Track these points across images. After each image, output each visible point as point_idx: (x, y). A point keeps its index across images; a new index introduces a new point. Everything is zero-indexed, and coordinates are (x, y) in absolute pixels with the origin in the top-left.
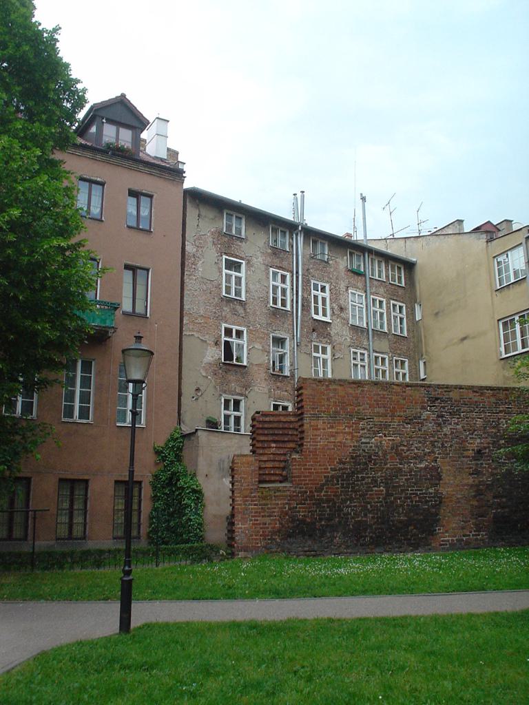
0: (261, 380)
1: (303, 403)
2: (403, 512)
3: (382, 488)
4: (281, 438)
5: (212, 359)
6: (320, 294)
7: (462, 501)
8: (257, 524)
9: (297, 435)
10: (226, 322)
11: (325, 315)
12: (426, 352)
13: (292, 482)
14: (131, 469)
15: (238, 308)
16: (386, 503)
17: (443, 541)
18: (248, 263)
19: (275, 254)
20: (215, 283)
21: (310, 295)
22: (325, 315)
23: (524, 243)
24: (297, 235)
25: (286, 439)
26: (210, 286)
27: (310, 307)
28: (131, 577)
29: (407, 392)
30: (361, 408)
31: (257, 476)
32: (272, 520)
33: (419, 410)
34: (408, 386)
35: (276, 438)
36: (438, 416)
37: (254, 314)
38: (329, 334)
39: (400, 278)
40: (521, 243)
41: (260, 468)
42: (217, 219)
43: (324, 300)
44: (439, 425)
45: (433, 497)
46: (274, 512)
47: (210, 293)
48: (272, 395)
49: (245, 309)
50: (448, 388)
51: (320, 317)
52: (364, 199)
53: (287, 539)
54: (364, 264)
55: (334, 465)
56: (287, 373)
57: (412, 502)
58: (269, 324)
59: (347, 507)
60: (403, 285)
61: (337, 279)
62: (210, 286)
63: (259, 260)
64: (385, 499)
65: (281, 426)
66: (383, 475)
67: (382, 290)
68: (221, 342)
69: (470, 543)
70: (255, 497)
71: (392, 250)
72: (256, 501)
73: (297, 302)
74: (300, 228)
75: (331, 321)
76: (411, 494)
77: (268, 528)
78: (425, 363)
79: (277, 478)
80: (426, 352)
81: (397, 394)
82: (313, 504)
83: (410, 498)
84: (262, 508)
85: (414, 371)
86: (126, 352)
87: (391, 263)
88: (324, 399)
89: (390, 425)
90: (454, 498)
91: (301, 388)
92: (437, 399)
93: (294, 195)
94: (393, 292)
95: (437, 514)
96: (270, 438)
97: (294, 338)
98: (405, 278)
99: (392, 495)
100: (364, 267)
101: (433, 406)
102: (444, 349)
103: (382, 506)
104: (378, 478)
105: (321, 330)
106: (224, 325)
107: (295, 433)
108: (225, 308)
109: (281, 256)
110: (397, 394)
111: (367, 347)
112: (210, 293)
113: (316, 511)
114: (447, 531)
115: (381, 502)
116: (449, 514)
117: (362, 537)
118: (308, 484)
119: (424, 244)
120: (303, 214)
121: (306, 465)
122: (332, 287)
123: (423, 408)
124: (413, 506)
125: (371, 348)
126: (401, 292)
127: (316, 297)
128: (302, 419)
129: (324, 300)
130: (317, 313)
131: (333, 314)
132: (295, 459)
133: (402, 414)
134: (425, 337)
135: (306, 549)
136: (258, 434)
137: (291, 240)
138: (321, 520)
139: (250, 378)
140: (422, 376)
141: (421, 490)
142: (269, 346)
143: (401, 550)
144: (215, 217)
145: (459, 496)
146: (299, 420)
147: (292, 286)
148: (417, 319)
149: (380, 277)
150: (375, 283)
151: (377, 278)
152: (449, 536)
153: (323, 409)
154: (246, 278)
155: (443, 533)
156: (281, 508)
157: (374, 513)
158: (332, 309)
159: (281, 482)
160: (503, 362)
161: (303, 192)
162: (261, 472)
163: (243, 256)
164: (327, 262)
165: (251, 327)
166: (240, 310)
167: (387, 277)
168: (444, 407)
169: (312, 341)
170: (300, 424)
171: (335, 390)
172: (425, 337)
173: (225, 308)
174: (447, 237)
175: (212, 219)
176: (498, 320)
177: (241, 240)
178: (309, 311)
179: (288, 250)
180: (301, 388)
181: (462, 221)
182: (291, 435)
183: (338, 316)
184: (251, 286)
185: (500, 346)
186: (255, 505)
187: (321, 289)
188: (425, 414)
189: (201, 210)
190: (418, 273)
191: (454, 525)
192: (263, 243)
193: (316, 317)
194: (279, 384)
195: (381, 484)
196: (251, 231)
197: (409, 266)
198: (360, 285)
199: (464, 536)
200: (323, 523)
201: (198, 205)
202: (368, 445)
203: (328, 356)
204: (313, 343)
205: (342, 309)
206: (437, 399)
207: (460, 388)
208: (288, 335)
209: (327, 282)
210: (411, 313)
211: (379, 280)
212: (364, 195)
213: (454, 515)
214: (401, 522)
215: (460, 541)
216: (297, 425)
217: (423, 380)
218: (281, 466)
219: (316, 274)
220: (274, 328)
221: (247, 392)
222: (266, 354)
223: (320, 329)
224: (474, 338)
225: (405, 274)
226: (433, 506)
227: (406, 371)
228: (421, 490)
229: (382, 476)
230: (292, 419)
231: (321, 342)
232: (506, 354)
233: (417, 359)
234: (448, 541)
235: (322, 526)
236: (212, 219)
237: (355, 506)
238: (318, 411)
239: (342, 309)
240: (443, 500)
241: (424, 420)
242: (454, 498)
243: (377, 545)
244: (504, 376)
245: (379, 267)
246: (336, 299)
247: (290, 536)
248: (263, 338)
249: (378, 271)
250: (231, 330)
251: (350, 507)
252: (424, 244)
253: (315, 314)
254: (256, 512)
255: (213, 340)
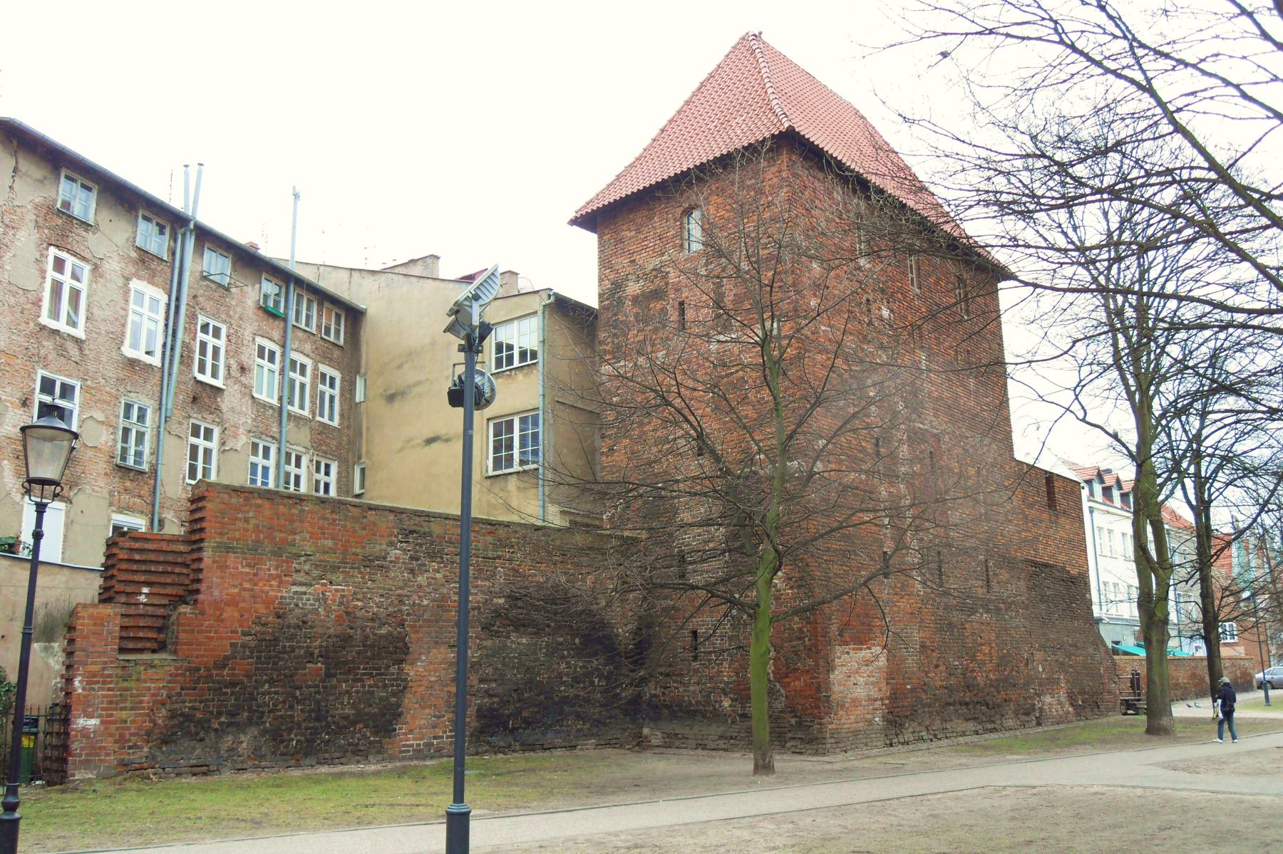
0: (98, 474)
1: (204, 525)
2: (349, 703)
3: (319, 665)
4: (162, 579)
5: (13, 430)
6: (210, 340)
7: (437, 687)
8: (110, 722)
9: (188, 575)
10: (45, 367)
11: (214, 375)
12: (368, 452)
13: (175, 652)
14: (27, 631)
15: (70, 346)
16: (324, 687)
17: (404, 746)
18: (96, 268)
19: (143, 261)
20: (31, 297)
21: (194, 339)
22: (214, 375)
23: (540, 313)
24: (184, 235)
25: (169, 581)
26: (23, 299)
27: (192, 359)
28: (17, 815)
29: (369, 518)
30: (297, 537)
31: (117, 641)
32: (137, 715)
33: (384, 547)
34: (370, 509)
35: (152, 578)
36: (412, 558)
37: (97, 360)
38: (218, 409)
39: (337, 332)
40: (536, 313)
41: (123, 628)
42: (46, 182)
43: (216, 350)
44: (412, 571)
45: (394, 680)
46: (141, 702)
47: (22, 313)
48: (116, 502)
49: (81, 350)
50: (428, 516)
51: (207, 378)
52: (296, 196)
53: (160, 748)
54: (286, 301)
55: (249, 627)
56: (145, 467)
57: (364, 686)
58: (120, 381)
59: (263, 694)
60: (341, 342)
61: (241, 319)
62: (23, 299)
63: (113, 266)
64: (322, 681)
65: (161, 559)
66: (324, 644)
67: (308, 347)
68: (32, 403)
69: (442, 748)
70: (110, 676)
71: (328, 284)
72: (111, 683)
73: (172, 349)
74: (192, 226)
75: (224, 387)
76: (362, 674)
77: (128, 728)
78: (363, 471)
79: (148, 645)
80: (368, 452)
81: (355, 519)
82: (209, 689)
83: (361, 680)
84: (121, 695)
85: (345, 482)
86: (28, 431)
87: (327, 304)
88: (240, 520)
89: (339, 568)
90: (425, 683)
91: (202, 498)
92: (412, 532)
93: (186, 166)
94: (325, 352)
95: (399, 706)
96: (143, 578)
97: (160, 409)
98: (345, 333)
99: (334, 676)
100: (286, 307)
101: (499, 558)
102: (399, 451)
103: (318, 693)
104: (316, 648)
105: (206, 400)
106: (41, 373)
107: (185, 571)
108: (45, 343)
109: (153, 267)
110: (355, 519)
111: (277, 436)
112: (22, 313)
113: (214, 700)
114: (411, 731)
115: (317, 686)
116: (416, 706)
117: (283, 742)
118: (203, 656)
119: (383, 285)
120: (195, 203)
121: (202, 625)
122: (232, 331)
123: (391, 544)
124: (364, 693)
125: (284, 438)
126: (337, 353)
127: (203, 345)
128: (200, 549)
129: (216, 350)
130: (202, 370)
131: (228, 376)
132: (185, 614)
133: (358, 550)
134: (368, 429)
135: (193, 762)
136: (119, 570)
137: (172, 244)
138: (219, 714)
139: (79, 469)
140: (357, 490)
141: (379, 669)
142: (117, 417)
143: (342, 760)
144: (45, 178)
145: (433, 679)
146: (193, 550)
147: (167, 319)
148: (357, 400)
149: (307, 325)
150: (300, 334)
151: (303, 326)
152: (414, 739)
153: (237, 534)
154: (89, 297)
155: (405, 734)
156: (154, 695)
157: (304, 705)
158: (228, 367)
159: (154, 651)
160: (489, 482)
161: (202, 165)
162: (124, 634)
163: (88, 256)
164: (227, 289)
165: (89, 383)
166: (73, 351)
167: (319, 327)
168: (421, 545)
169: (190, 417)
170: (195, 556)
171: (259, 506)
172: (368, 429)
173: (45, 343)
174: (421, 280)
175: (39, 181)
176: (488, 420)
177: (86, 225)
178: (189, 366)
179: (165, 258)
180: (202, 498)
181: (438, 258)
182: (179, 574)
183: (237, 381)
184: (96, 311)
185: (487, 458)
186: (109, 689)
187: (202, 327)
188: (394, 553)
189: (21, 161)
190: (366, 333)
191: (423, 722)
192: (124, 241)
193: (200, 377)
194: (128, 484)
195: (320, 659)
196: (105, 215)
197: (353, 316)
198: (276, 335)
199: (435, 738)
200: (223, 719)
201: (16, 152)
202: (305, 597)
203: (214, 445)
204: (192, 421)
205: (243, 369)
206: (412, 532)
207: (446, 518)
208: (152, 402)
209: (224, 322)
210: (349, 389)
211: (305, 331)
212: (297, 190)
213: (423, 708)
214: (346, 718)
215: (429, 745)
216: (188, 558)
217: (358, 496)
218: (158, 625)
219: (209, 305)
220: (129, 388)
221: (72, 494)
222: (111, 430)
223: (204, 397)
224: (447, 440)
225: (346, 327)
226: (394, 694)
227: (333, 479)
228: (379, 669)
229: (321, 647)
230: (182, 548)
231: (204, 419)
232: (494, 470)
233: (351, 463)
234: (412, 746)
235: (221, 724)
236: (39, 181)
237: (276, 693)
238: (228, 538)
239: (243, 369)
240: (410, 684)
241: (391, 562)
242: (425, 683)
243: (306, 755)
244: (489, 503)
245: (308, 309)
246: (236, 352)
247: (165, 742)
248: (108, 403)
249: (310, 318)
250: (53, 382)
251: (269, 693)
252: (383, 285)
253: (199, 372)
254: (111, 702)
255: (18, 396)
